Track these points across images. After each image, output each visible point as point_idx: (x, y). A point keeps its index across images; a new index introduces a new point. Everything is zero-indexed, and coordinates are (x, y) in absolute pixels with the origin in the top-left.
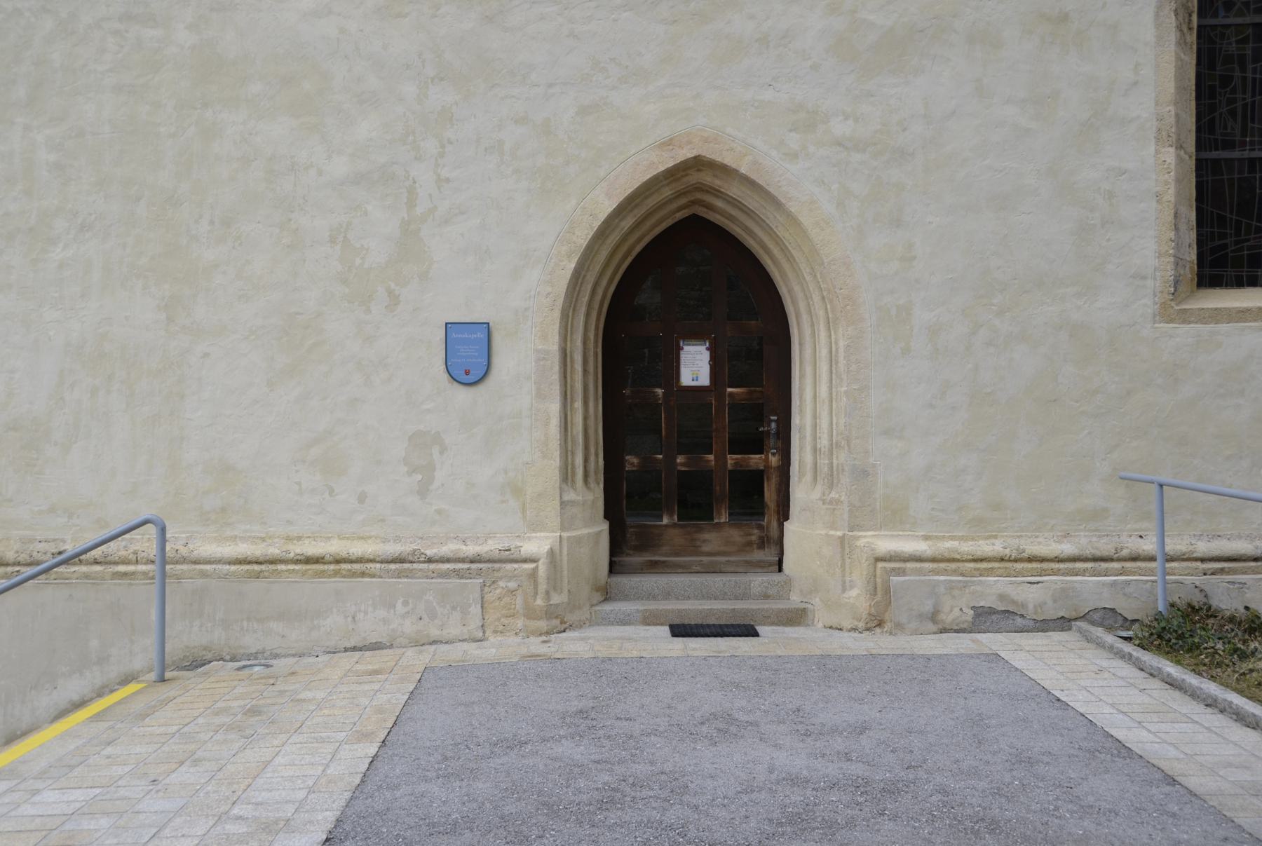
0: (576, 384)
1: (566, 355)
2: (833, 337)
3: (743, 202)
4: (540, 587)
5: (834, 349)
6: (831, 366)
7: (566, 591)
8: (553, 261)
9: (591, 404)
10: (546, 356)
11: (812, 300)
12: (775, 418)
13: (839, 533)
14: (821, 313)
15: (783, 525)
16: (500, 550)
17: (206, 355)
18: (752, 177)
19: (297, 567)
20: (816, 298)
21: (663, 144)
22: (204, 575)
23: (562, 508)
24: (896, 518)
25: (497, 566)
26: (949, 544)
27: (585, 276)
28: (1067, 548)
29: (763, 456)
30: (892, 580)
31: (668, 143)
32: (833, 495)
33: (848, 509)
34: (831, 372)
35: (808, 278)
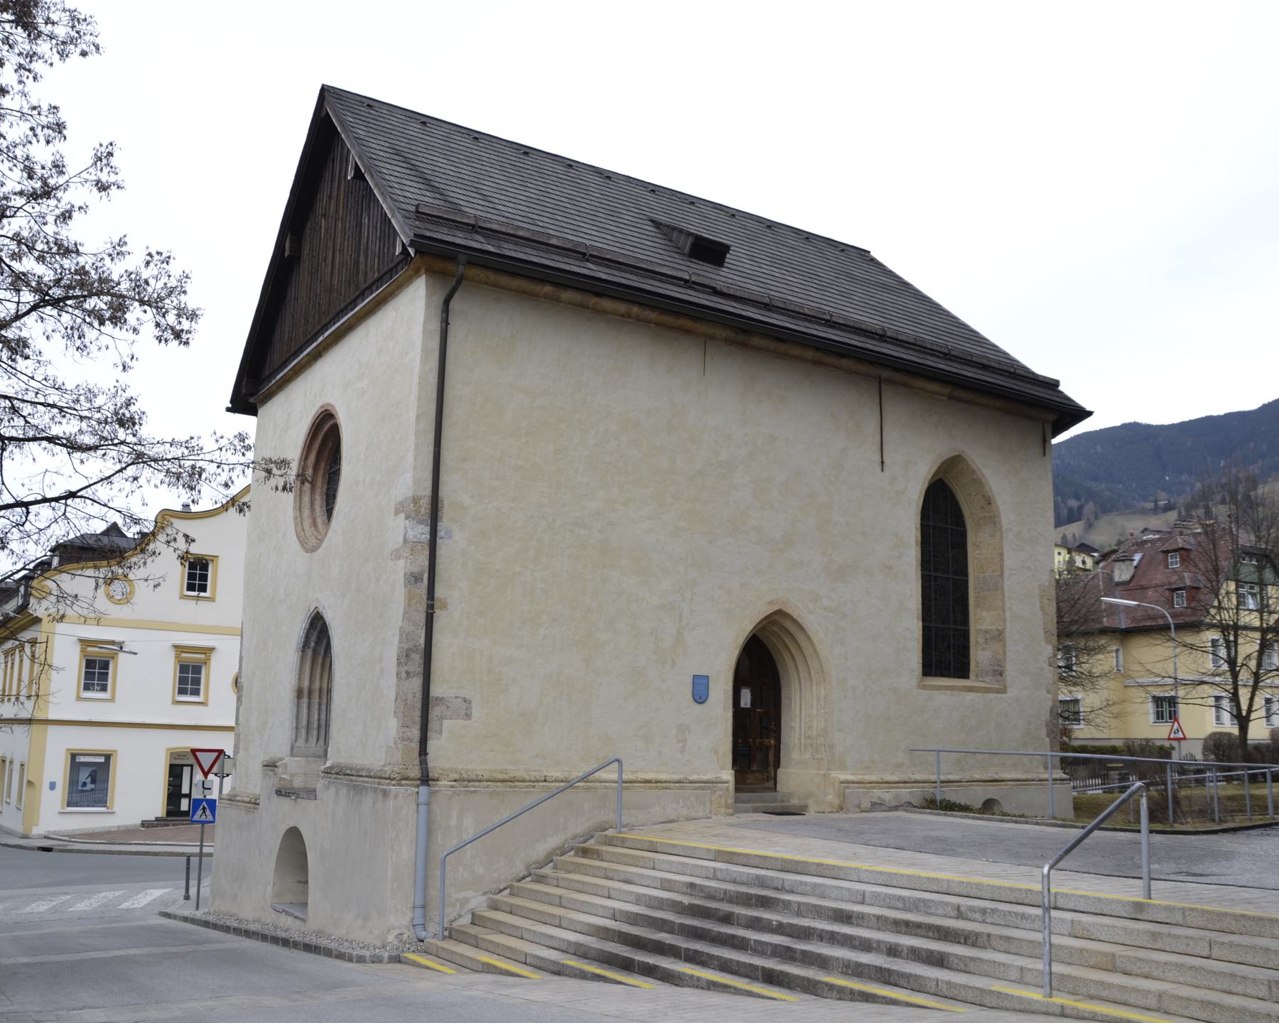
17: (601, 684)
19: (641, 785)
22: (606, 788)
24: (842, 766)
26: (860, 777)
28: (895, 778)
31: (770, 603)
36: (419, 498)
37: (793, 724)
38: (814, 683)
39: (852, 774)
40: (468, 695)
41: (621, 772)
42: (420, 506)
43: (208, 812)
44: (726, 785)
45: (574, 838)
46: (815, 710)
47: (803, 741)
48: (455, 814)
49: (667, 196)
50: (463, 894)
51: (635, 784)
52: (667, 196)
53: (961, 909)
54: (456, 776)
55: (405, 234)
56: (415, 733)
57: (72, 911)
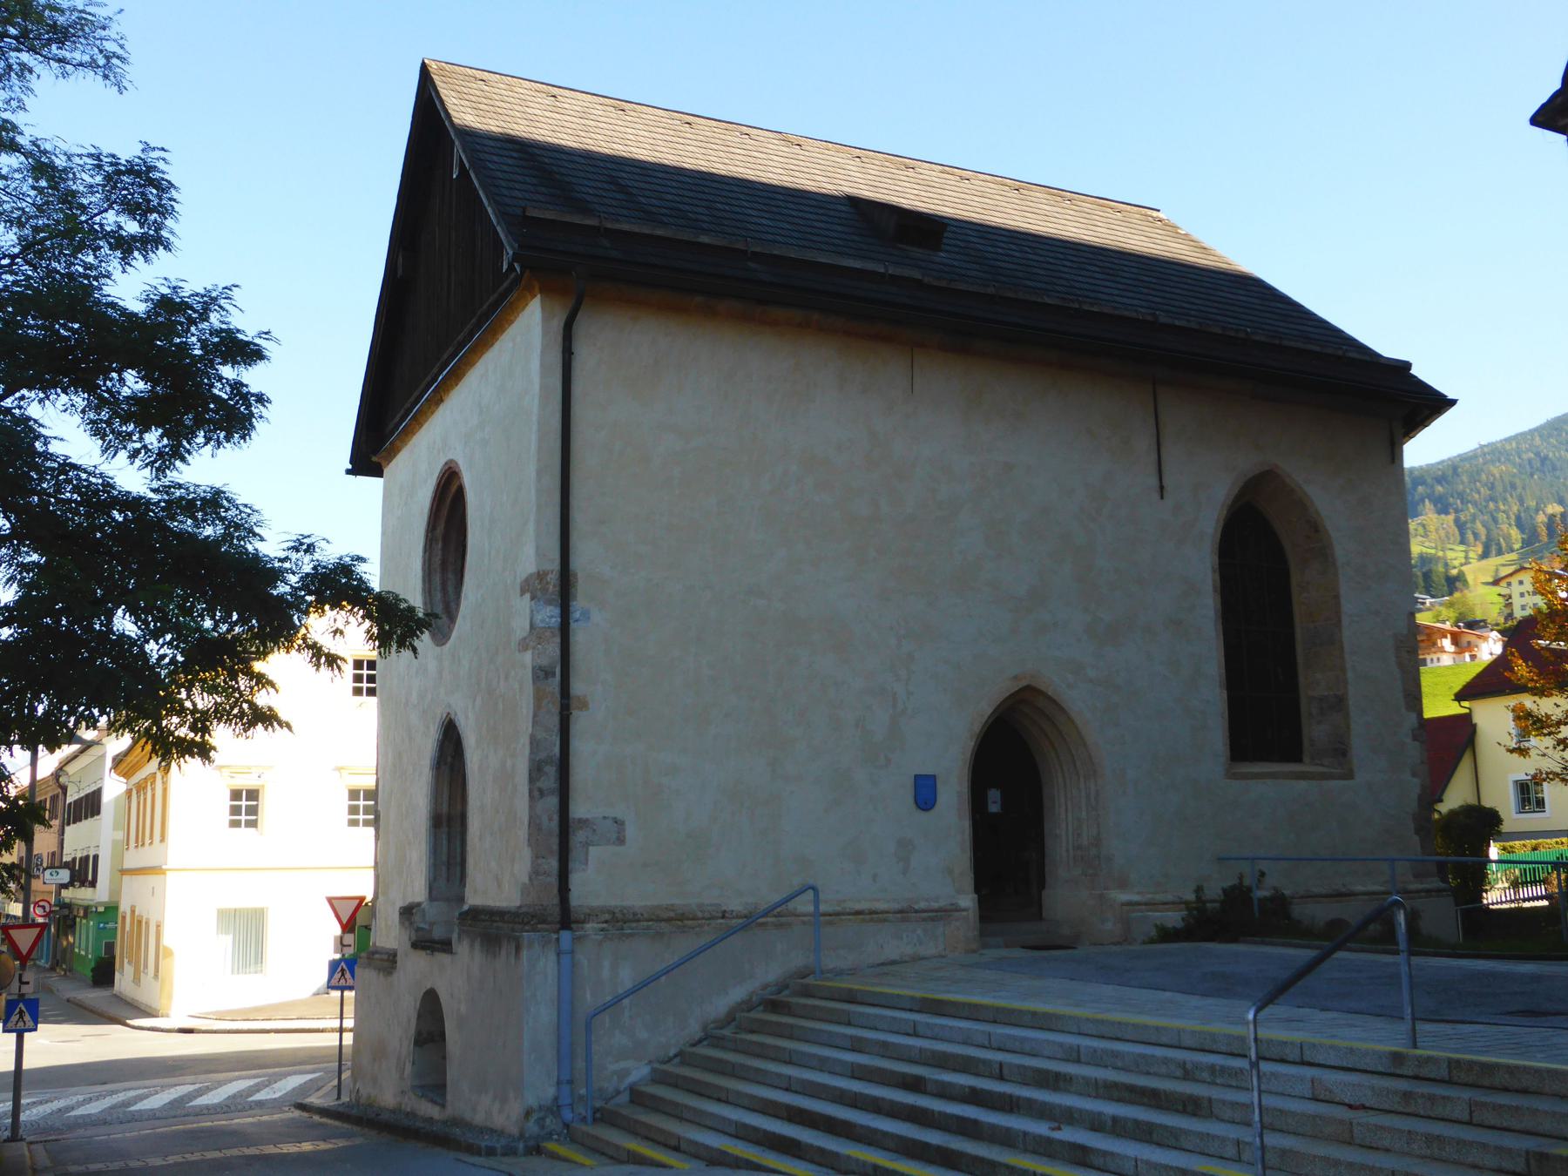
19: (850, 917)
24: (1123, 884)
26: (1150, 896)
31: (1016, 678)
36: (546, 574)
37: (1058, 832)
38: (1082, 780)
39: (1138, 893)
40: (619, 816)
41: (817, 902)
42: (547, 583)
43: (348, 975)
44: (965, 913)
45: (765, 987)
46: (1084, 813)
47: (1071, 851)
48: (606, 964)
49: (877, 163)
50: (623, 1064)
51: (843, 917)
52: (877, 163)
53: (1187, 1066)
54: (607, 917)
55: (512, 247)
56: (553, 864)
57: (192, 1106)
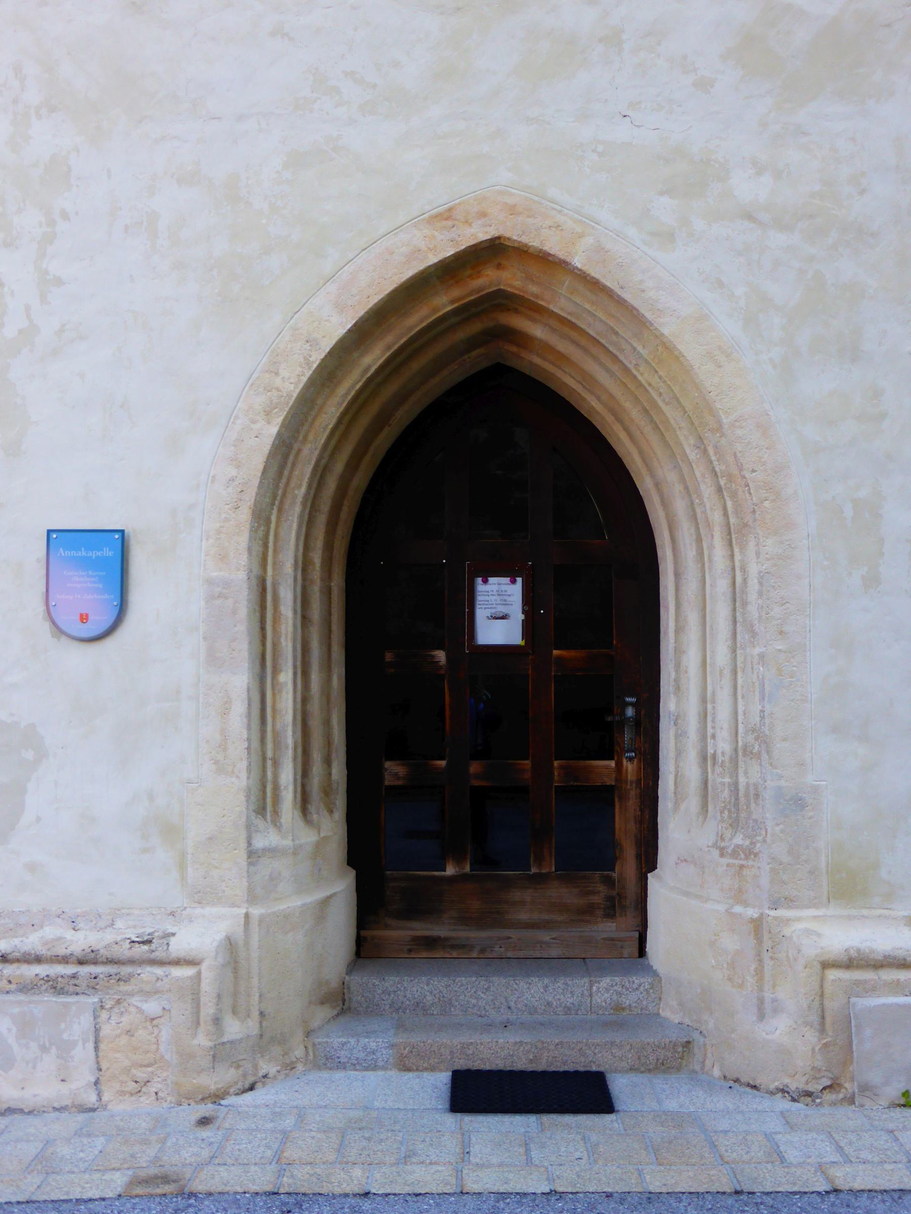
0: (283, 640)
1: (263, 590)
2: (738, 557)
3: (579, 323)
4: (203, 1013)
5: (739, 580)
6: (734, 610)
7: (255, 1014)
8: (239, 422)
9: (315, 678)
10: (224, 591)
11: (700, 496)
12: (634, 700)
13: (752, 913)
14: (716, 517)
15: (647, 879)
16: (133, 942)
18: (593, 274)
20: (707, 490)
21: (439, 217)
23: (250, 864)
25: (126, 970)
27: (299, 451)
29: (612, 764)
30: (854, 1004)
32: (739, 840)
33: (768, 867)
34: (735, 621)
35: (693, 455)
